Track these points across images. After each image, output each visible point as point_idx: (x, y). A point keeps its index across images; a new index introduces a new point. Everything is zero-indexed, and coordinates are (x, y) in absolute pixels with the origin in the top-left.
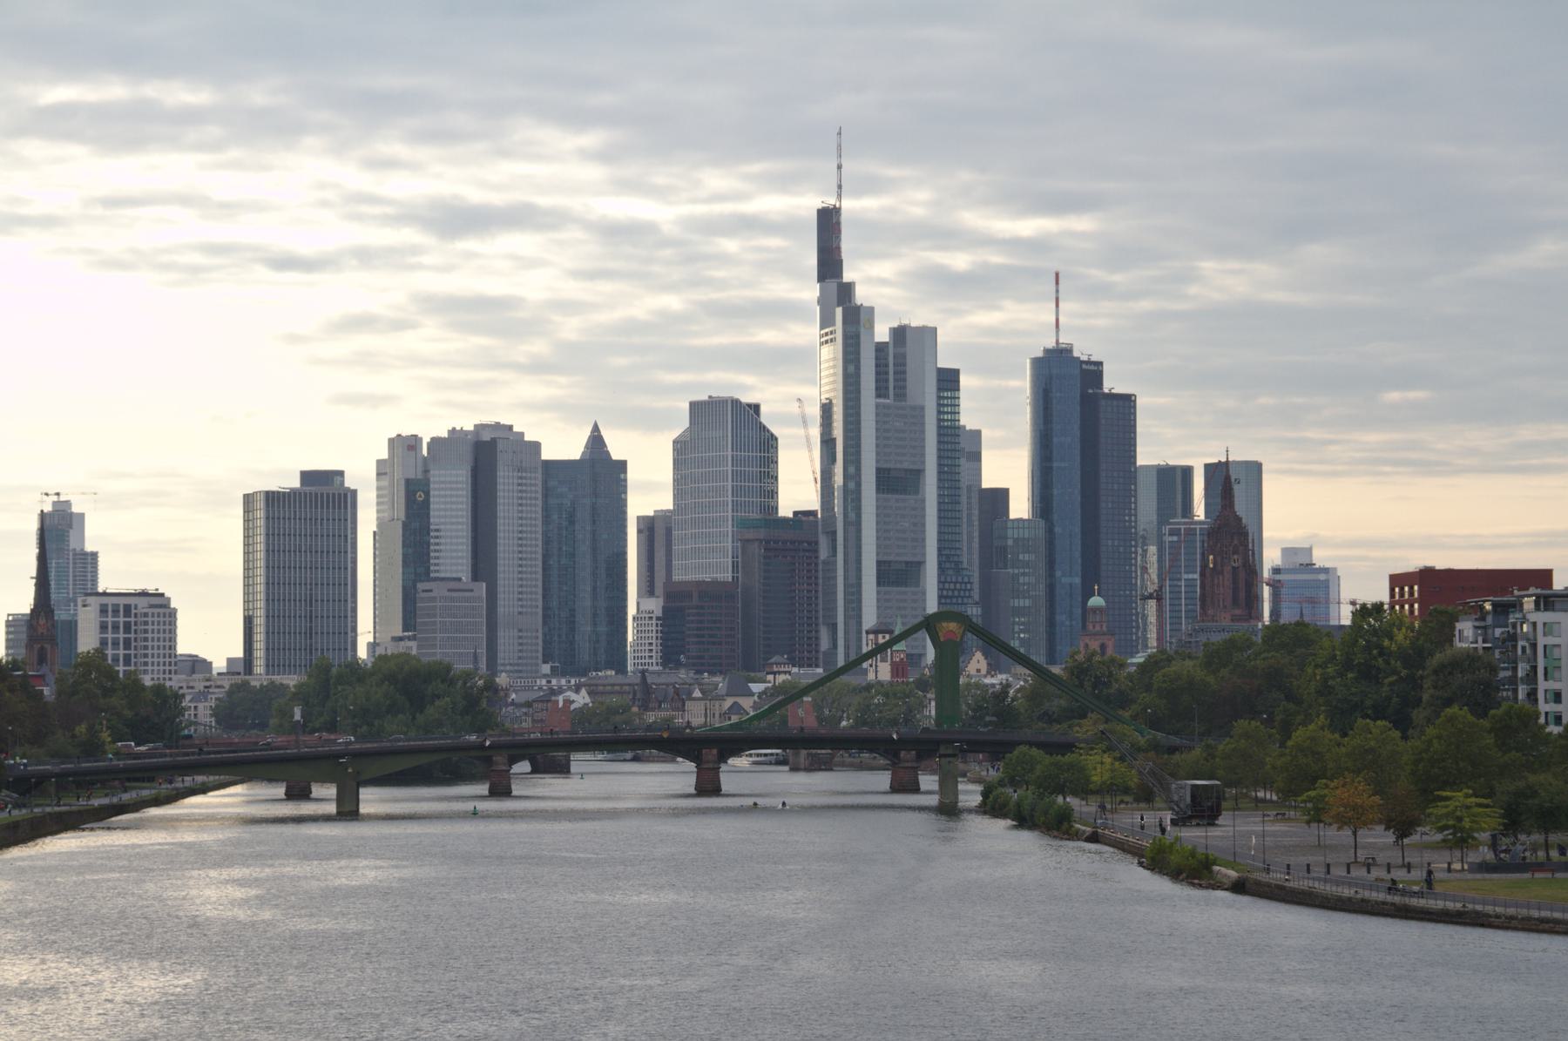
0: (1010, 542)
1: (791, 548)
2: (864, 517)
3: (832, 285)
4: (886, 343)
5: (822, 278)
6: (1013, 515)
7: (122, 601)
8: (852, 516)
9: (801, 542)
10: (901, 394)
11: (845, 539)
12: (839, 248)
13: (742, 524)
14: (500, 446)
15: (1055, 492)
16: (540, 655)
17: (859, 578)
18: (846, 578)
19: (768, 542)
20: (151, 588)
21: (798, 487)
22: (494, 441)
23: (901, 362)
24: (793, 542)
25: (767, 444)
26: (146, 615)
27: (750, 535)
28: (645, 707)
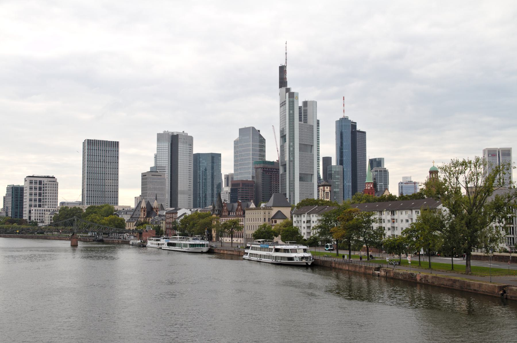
0: (333, 172)
1: (270, 173)
2: (295, 159)
3: (284, 89)
4: (301, 107)
5: (281, 87)
6: (332, 165)
7: (38, 179)
8: (292, 159)
9: (274, 169)
10: (306, 121)
11: (289, 166)
12: (286, 78)
13: (256, 163)
14: (179, 137)
15: (344, 158)
16: (192, 205)
17: (294, 178)
18: (289, 179)
19: (264, 168)
20: (51, 175)
21: (272, 154)
22: (177, 135)
23: (306, 111)
24: (271, 169)
25: (262, 141)
26: (46, 184)
27: (258, 166)
28: (220, 214)
